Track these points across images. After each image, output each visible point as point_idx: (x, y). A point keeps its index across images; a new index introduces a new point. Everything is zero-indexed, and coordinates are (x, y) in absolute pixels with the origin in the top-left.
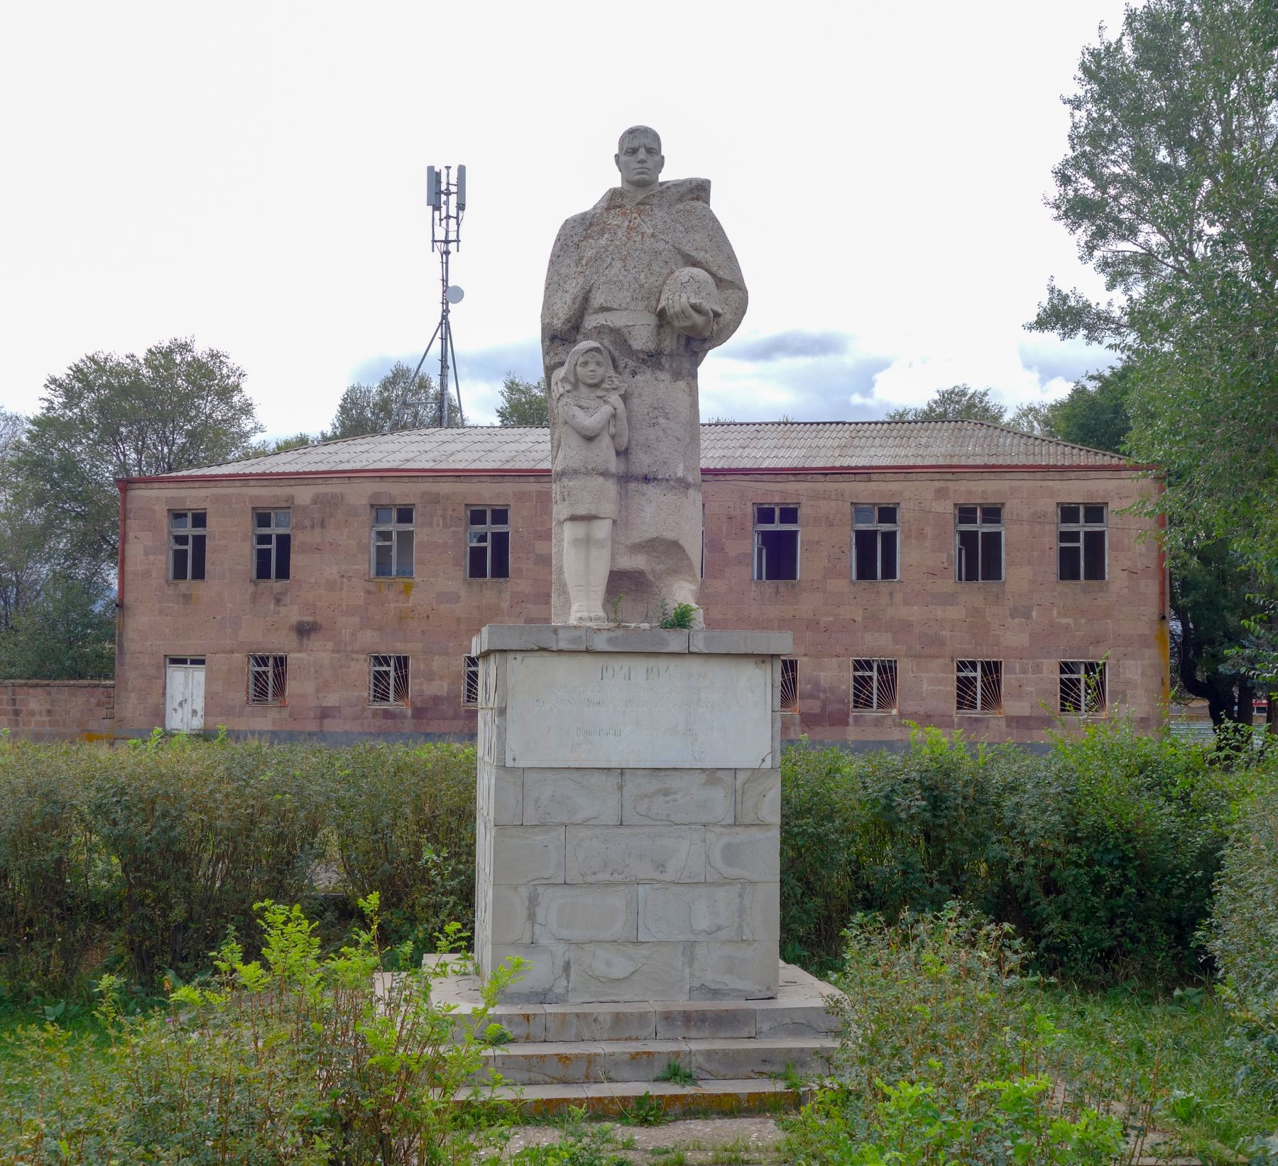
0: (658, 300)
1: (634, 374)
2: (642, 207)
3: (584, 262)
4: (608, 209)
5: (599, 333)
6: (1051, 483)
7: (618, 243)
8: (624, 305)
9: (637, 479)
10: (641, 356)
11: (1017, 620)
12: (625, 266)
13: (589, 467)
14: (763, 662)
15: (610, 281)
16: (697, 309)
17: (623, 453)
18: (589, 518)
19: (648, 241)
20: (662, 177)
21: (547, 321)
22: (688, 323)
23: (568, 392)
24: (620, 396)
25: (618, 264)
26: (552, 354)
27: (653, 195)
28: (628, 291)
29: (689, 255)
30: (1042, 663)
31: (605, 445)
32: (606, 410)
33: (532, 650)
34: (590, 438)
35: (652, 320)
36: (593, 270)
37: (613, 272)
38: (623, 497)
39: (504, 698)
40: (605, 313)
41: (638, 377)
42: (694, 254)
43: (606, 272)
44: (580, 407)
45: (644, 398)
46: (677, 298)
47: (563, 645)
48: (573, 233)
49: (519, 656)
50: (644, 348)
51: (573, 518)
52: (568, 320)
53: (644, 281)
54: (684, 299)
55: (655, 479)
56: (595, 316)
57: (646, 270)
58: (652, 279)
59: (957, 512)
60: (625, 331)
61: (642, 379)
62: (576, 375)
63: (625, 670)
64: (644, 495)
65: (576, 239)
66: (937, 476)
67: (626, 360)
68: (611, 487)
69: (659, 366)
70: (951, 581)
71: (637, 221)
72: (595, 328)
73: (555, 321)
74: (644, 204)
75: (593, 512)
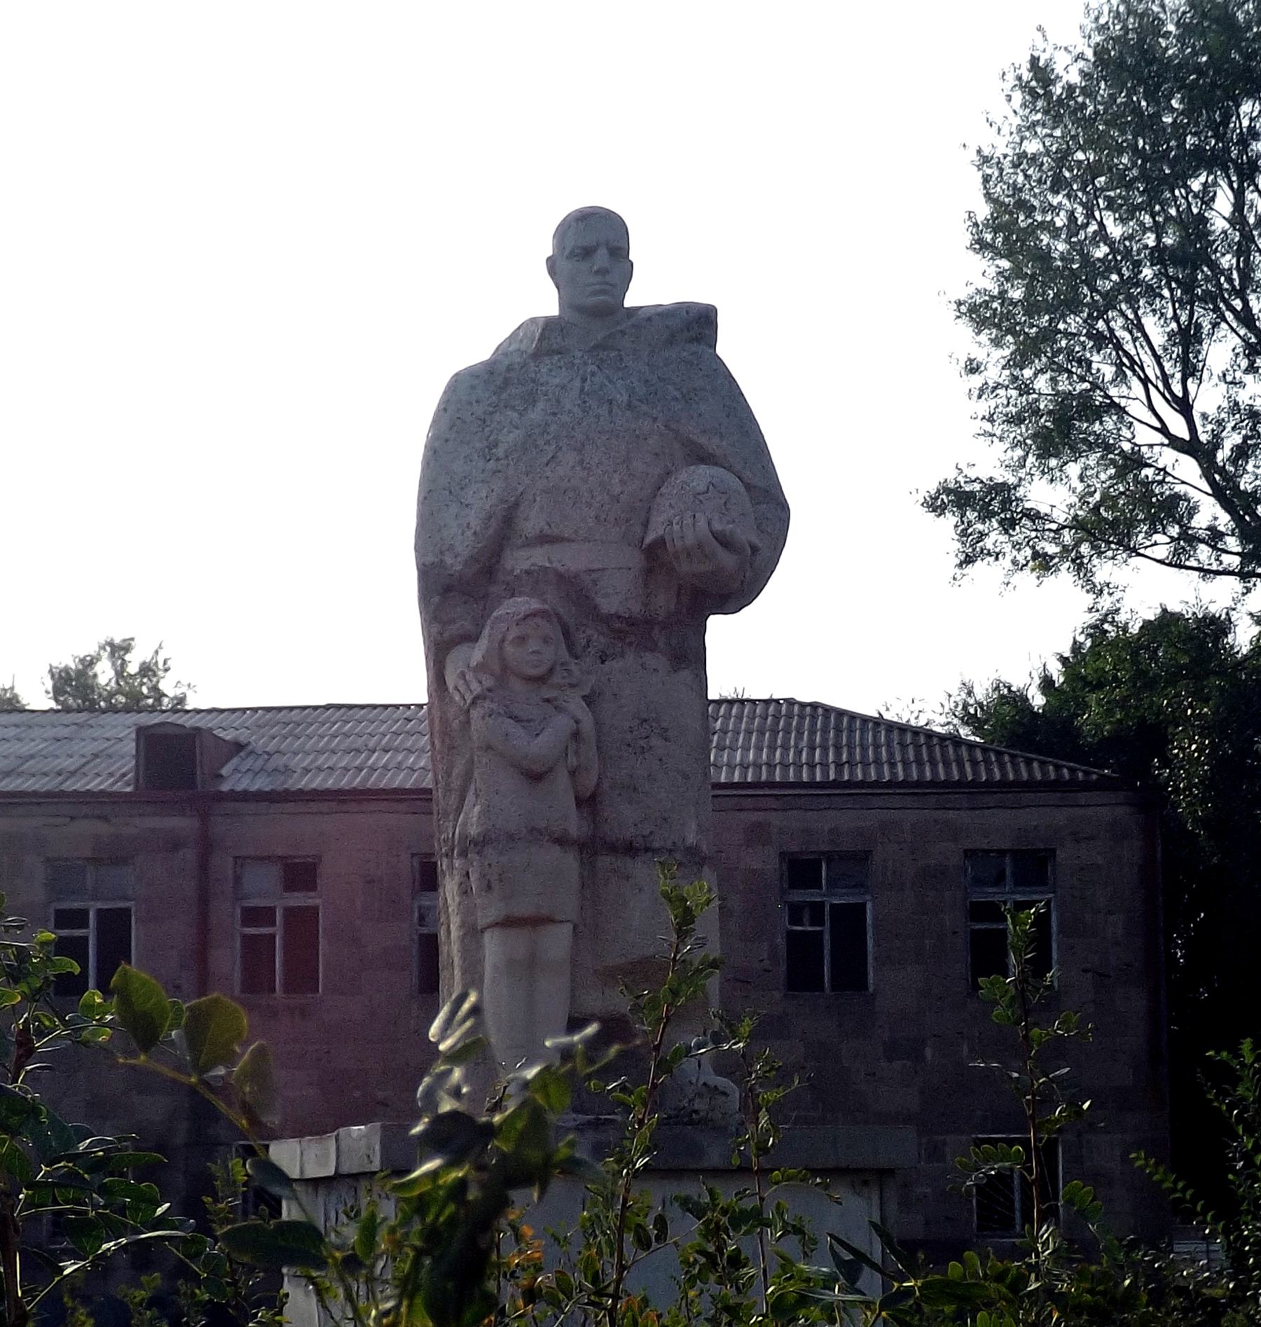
0: (646, 525)
2: (603, 355)
3: (500, 451)
4: (537, 355)
6: (951, 814)
7: (565, 418)
9: (613, 848)
11: (897, 1065)
12: (581, 462)
14: (865, 1183)
16: (725, 541)
17: (588, 803)
18: (536, 922)
20: (630, 301)
21: (430, 559)
22: (704, 567)
23: (490, 690)
24: (584, 698)
25: (570, 458)
27: (623, 333)
28: (589, 505)
30: (945, 1144)
31: (561, 788)
32: (562, 724)
34: (535, 777)
35: (635, 560)
38: (589, 882)
41: (610, 664)
42: (703, 440)
46: (688, 521)
51: (508, 923)
52: (473, 559)
53: (618, 490)
54: (702, 523)
56: (523, 553)
59: (785, 867)
62: (502, 659)
64: (627, 878)
65: (479, 410)
66: (748, 803)
68: (570, 862)
70: (777, 995)
71: (597, 379)
72: (528, 572)
73: (449, 560)
75: (544, 911)
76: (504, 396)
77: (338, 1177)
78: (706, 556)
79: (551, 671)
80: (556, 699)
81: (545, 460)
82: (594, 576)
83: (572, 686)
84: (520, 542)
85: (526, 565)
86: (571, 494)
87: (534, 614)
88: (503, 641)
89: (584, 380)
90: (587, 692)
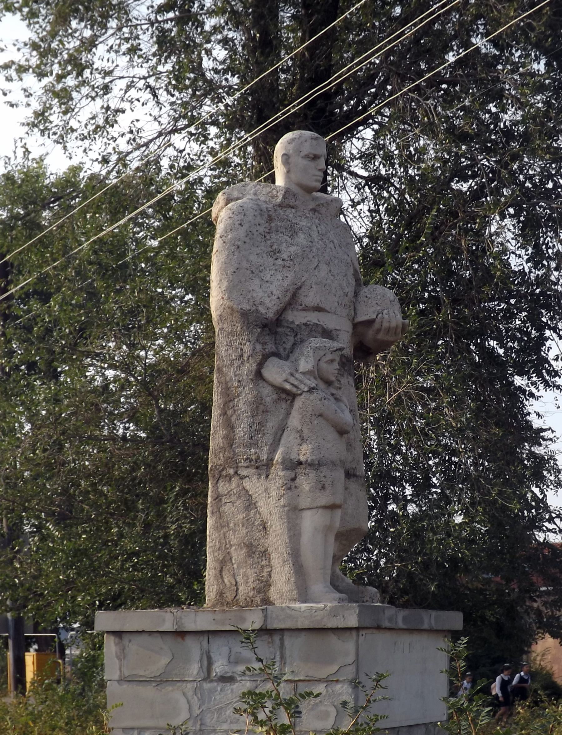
12: (330, 271)
25: (324, 268)
40: (316, 313)
56: (305, 314)
65: (261, 229)
72: (306, 325)
81: (314, 266)
82: (338, 332)
84: (300, 308)
85: (304, 321)
88: (319, 360)
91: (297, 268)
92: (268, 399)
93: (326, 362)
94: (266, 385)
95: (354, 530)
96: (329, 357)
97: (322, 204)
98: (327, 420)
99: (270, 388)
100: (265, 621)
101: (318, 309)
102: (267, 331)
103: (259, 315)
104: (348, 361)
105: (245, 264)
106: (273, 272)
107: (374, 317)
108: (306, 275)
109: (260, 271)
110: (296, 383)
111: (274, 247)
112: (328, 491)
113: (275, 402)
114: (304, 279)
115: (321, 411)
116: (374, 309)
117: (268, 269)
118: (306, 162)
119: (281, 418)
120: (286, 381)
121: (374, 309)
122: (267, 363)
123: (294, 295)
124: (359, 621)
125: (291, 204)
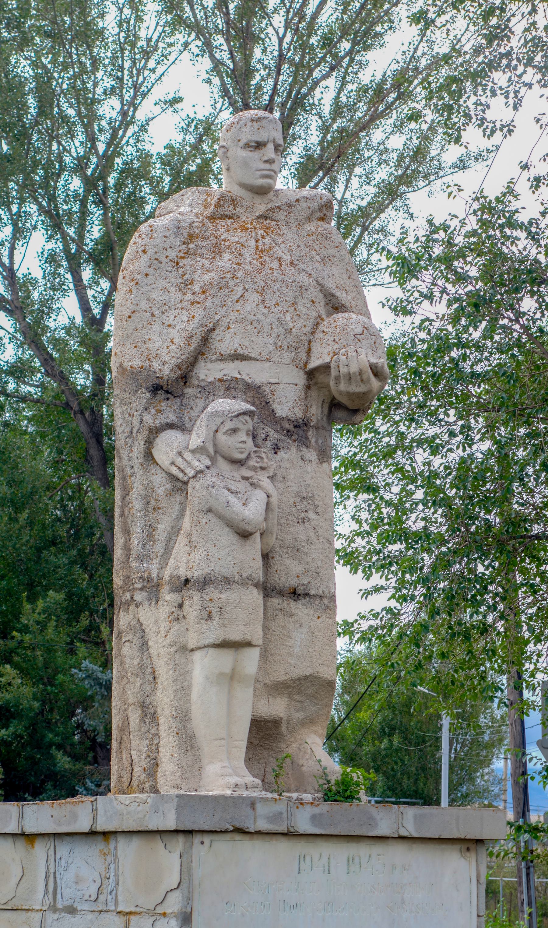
1: (276, 449)
5: (228, 388)
8: (265, 355)
9: (281, 593)
10: (287, 425)
12: (263, 301)
13: (245, 575)
14: (468, 849)
15: (244, 319)
19: (290, 271)
22: (362, 389)
23: (208, 467)
25: (254, 298)
26: (153, 411)
29: (333, 295)
33: (226, 832)
35: (301, 379)
36: (217, 301)
37: (248, 307)
39: (189, 899)
40: (237, 363)
41: (281, 454)
43: (238, 306)
44: (229, 490)
45: (289, 483)
47: (263, 825)
48: (166, 245)
49: (207, 839)
50: (290, 415)
55: (306, 595)
56: (220, 365)
57: (291, 310)
58: (300, 323)
60: (267, 389)
61: (286, 456)
63: (324, 860)
64: (291, 615)
65: (173, 254)
67: (267, 429)
69: (304, 442)
72: (220, 380)
74: (266, 218)
76: (191, 246)
77: (92, 834)
78: (362, 381)
79: (248, 457)
80: (251, 477)
81: (235, 298)
82: (273, 387)
83: (263, 469)
84: (214, 357)
85: (219, 376)
86: (255, 324)
87: (244, 413)
88: (217, 431)
89: (257, 241)
90: (271, 474)
91: (208, 304)
92: (161, 491)
93: (225, 433)
94: (159, 471)
95: (305, 678)
96: (229, 425)
97: (278, 207)
98: (220, 517)
99: (164, 475)
100: (95, 819)
101: (237, 357)
102: (161, 395)
103: (151, 373)
104: (295, 427)
105: (144, 305)
106: (178, 311)
107: (328, 359)
108: (222, 311)
109: (163, 313)
110: (182, 465)
111: (186, 277)
112: (215, 622)
113: (169, 494)
114: (217, 317)
115: (209, 504)
116: (330, 348)
117: (173, 307)
118: (245, 153)
119: (174, 517)
120: (173, 463)
121: (330, 348)
122: (158, 440)
123: (205, 340)
124: (177, 819)
125: (228, 213)
